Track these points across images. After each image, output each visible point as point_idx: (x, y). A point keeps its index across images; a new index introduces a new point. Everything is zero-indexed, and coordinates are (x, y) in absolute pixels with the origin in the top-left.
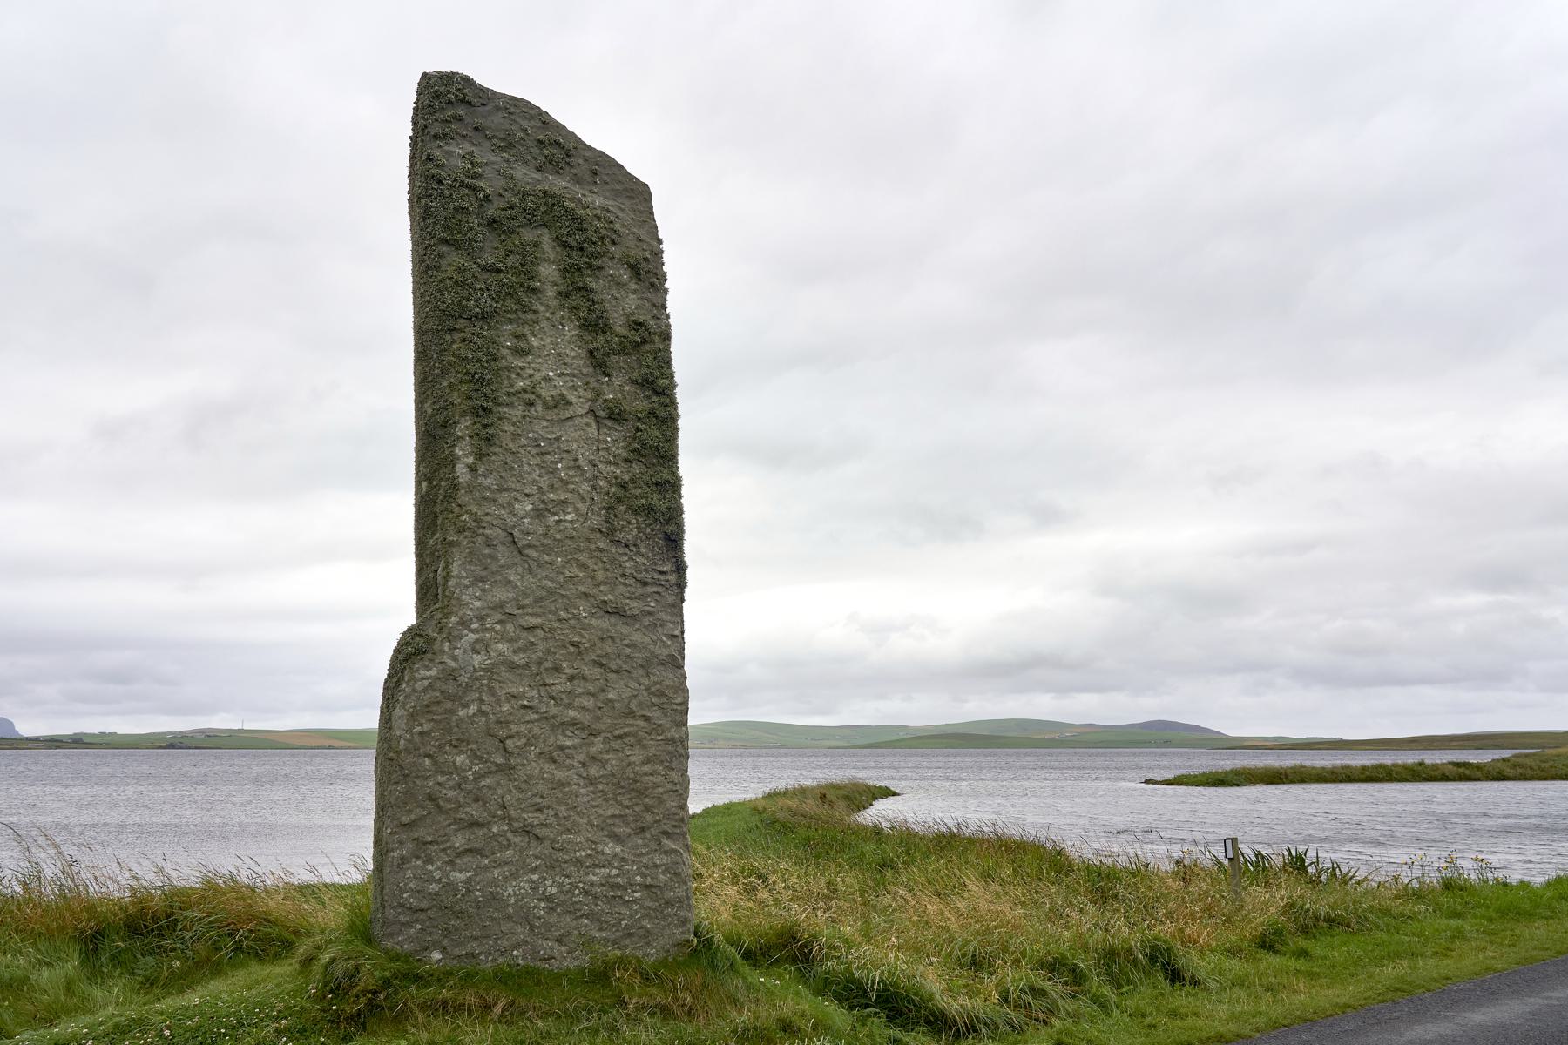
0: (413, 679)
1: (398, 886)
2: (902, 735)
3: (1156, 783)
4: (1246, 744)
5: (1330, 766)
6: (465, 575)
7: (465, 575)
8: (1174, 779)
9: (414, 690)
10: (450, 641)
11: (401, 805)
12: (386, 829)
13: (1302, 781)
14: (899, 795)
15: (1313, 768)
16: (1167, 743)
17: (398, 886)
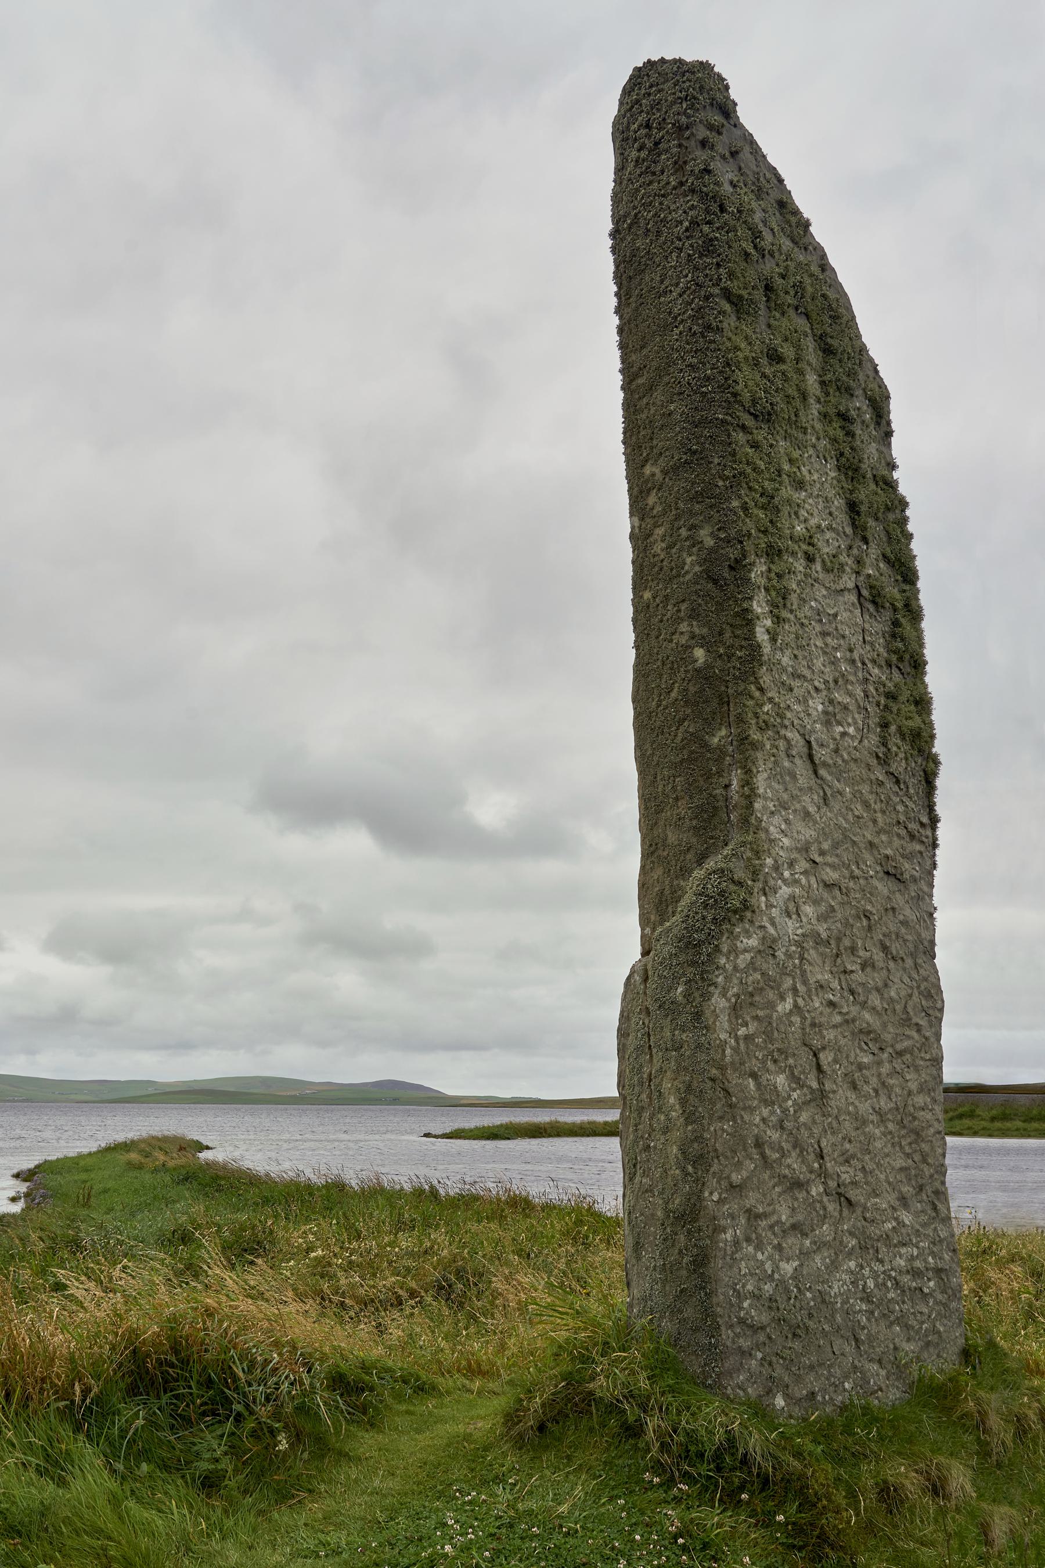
0: (734, 951)
1: (735, 1290)
2: (151, 1090)
3: (436, 1137)
4: (462, 1102)
5: (579, 1122)
6: (770, 795)
7: (770, 795)
8: (451, 1133)
9: (736, 968)
10: (765, 894)
11: (729, 1154)
12: (711, 1193)
13: (558, 1135)
14: (212, 1149)
15: (566, 1123)
16: (395, 1101)
17: (735, 1290)
